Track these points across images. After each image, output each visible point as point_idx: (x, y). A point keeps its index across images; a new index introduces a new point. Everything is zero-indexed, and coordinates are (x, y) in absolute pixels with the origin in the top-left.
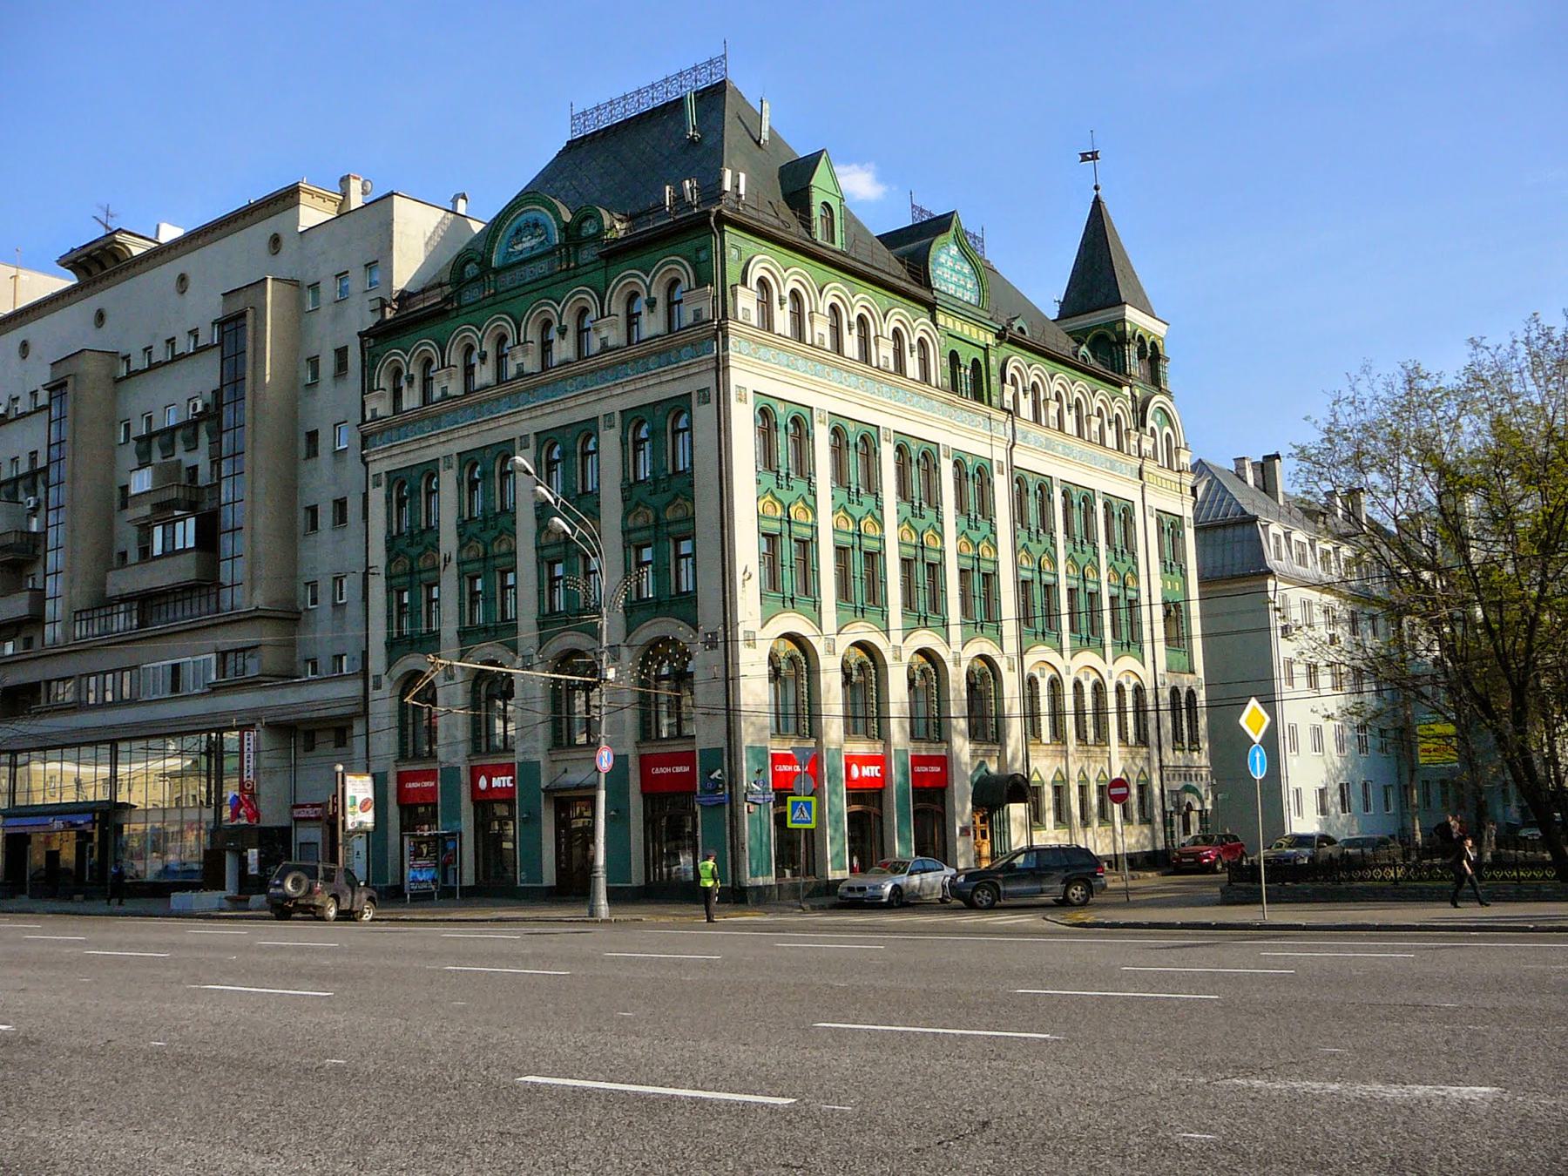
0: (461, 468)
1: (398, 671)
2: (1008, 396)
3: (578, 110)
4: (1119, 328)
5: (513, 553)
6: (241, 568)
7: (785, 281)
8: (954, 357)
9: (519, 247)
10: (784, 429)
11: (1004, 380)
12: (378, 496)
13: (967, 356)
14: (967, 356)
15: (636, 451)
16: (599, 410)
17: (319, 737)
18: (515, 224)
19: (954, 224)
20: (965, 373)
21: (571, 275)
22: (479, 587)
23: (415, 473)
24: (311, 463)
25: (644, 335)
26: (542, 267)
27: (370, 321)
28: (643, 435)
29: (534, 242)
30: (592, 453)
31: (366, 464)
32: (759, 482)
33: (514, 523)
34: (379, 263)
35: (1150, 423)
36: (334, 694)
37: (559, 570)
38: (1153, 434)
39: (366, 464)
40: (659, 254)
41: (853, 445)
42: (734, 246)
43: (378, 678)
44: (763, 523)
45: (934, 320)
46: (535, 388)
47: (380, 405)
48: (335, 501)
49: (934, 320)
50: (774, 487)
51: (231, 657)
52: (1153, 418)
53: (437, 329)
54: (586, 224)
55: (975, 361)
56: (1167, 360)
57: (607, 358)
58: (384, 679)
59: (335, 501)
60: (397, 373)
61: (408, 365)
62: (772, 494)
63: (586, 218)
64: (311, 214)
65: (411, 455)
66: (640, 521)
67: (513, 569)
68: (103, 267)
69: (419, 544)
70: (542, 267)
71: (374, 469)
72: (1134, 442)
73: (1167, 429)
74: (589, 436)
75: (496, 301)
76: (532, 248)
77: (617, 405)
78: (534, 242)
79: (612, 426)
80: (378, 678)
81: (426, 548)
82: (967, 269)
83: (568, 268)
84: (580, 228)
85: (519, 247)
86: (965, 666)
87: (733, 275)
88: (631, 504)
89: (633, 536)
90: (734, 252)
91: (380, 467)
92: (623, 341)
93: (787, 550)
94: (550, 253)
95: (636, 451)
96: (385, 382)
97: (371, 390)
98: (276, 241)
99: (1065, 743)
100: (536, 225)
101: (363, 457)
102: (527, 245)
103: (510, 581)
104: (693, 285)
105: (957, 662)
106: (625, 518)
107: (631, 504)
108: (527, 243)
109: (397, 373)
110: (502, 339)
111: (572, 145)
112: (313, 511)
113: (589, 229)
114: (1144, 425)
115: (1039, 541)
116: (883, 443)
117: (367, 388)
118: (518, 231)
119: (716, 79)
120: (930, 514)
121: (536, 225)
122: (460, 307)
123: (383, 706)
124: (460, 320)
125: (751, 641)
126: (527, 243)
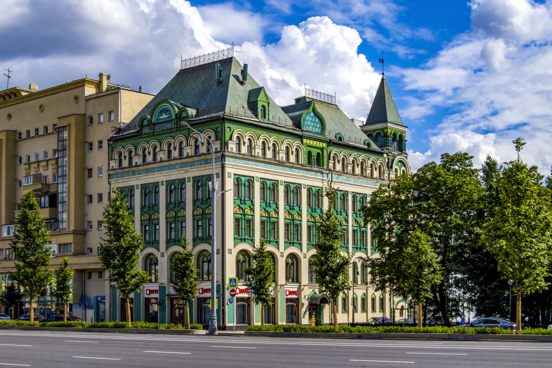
2: (331, 165)
3: (184, 59)
4: (385, 131)
5: (158, 219)
6: (65, 216)
8: (309, 153)
9: (161, 117)
10: (244, 185)
11: (329, 159)
13: (314, 152)
14: (314, 152)
15: (197, 190)
16: (186, 176)
17: (93, 274)
18: (160, 109)
19: (312, 105)
22: (147, 228)
23: (127, 189)
24: (90, 179)
25: (200, 152)
26: (169, 125)
27: (112, 134)
28: (200, 184)
29: (167, 116)
31: (110, 184)
32: (234, 202)
35: (395, 166)
37: (173, 225)
38: (396, 170)
39: (110, 184)
40: (205, 128)
41: (270, 188)
44: (235, 215)
45: (302, 142)
47: (114, 164)
48: (98, 194)
49: (302, 142)
50: (239, 204)
53: (134, 141)
55: (318, 154)
56: (406, 141)
57: (188, 160)
59: (98, 194)
60: (120, 154)
61: (124, 152)
62: (239, 206)
63: (183, 111)
64: (90, 90)
65: (125, 183)
66: (198, 213)
67: (158, 224)
68: (10, 98)
69: (206, 203)
70: (169, 125)
71: (227, 170)
72: (386, 175)
73: (403, 168)
75: (153, 135)
76: (166, 118)
77: (139, 182)
78: (167, 116)
82: (317, 120)
83: (177, 127)
84: (181, 114)
85: (161, 117)
86: (308, 257)
87: (227, 138)
88: (195, 207)
92: (193, 154)
93: (243, 224)
94: (171, 121)
95: (197, 190)
96: (117, 157)
97: (112, 159)
98: (76, 98)
102: (164, 117)
103: (157, 227)
105: (305, 257)
106: (193, 212)
107: (195, 207)
108: (164, 116)
109: (120, 154)
110: (155, 148)
112: (91, 197)
113: (184, 115)
114: (391, 167)
115: (341, 215)
116: (280, 186)
117: (110, 158)
120: (297, 209)
122: (142, 134)
124: (142, 140)
126: (164, 116)
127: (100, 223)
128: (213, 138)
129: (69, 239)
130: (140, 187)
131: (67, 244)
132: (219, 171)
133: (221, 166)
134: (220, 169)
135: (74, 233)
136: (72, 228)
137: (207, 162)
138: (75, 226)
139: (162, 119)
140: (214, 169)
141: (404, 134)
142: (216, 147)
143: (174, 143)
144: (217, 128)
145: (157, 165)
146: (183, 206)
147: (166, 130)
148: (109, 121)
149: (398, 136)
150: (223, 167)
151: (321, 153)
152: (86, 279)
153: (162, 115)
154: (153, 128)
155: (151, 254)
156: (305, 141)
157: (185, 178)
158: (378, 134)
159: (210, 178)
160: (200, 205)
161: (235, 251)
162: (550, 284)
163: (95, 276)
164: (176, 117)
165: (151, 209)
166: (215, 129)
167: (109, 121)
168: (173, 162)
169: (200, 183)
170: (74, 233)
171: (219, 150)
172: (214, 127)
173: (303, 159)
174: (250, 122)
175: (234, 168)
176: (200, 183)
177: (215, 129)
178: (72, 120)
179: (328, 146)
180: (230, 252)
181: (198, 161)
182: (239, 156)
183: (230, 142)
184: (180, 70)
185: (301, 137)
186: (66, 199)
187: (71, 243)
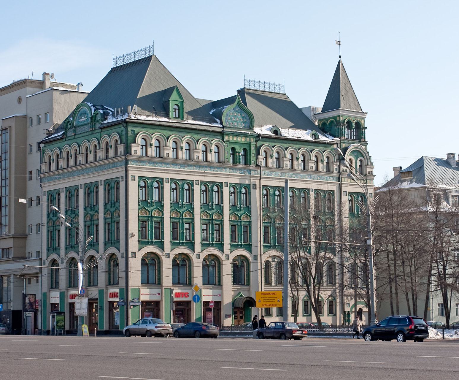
0: (66, 192)
1: (50, 259)
3: (115, 57)
4: (338, 119)
8: (233, 149)
9: (81, 120)
12: (45, 199)
24: (31, 181)
31: (42, 187)
33: (119, 206)
34: (49, 113)
36: (33, 265)
39: (42, 187)
43: (45, 261)
46: (83, 170)
49: (223, 139)
51: (5, 250)
58: (46, 261)
65: (54, 186)
69: (114, 207)
71: (131, 173)
77: (103, 178)
80: (45, 261)
81: (76, 216)
83: (92, 131)
85: (81, 120)
91: (45, 189)
99: (335, 315)
101: (41, 186)
102: (83, 120)
107: (106, 210)
111: (114, 70)
118: (81, 114)
121: (85, 113)
123: (46, 268)
124: (66, 142)
125: (134, 255)
126: (83, 119)
127: (39, 226)
128: (119, 142)
129: (9, 243)
130: (64, 189)
131: (8, 248)
133: (124, 169)
134: (124, 172)
135: (14, 237)
136: (12, 232)
137: (114, 165)
138: (15, 230)
140: (119, 173)
141: (363, 122)
144: (122, 131)
145: (79, 169)
146: (97, 210)
148: (45, 123)
149: (354, 124)
151: (248, 149)
152: (27, 285)
154: (75, 131)
155: (113, 254)
156: (226, 138)
158: (332, 122)
160: (109, 208)
161: (140, 255)
162: (283, 287)
163: (34, 280)
164: (92, 121)
165: (113, 205)
166: (120, 132)
167: (45, 123)
168: (80, 167)
169: (112, 186)
170: (14, 237)
172: (119, 130)
173: (226, 155)
174: (158, 123)
175: (136, 171)
176: (112, 186)
177: (120, 132)
178: (12, 124)
179: (256, 141)
180: (134, 255)
181: (107, 164)
182: (145, 159)
183: (133, 145)
184: (112, 69)
185: (222, 134)
186: (7, 203)
187: (12, 248)
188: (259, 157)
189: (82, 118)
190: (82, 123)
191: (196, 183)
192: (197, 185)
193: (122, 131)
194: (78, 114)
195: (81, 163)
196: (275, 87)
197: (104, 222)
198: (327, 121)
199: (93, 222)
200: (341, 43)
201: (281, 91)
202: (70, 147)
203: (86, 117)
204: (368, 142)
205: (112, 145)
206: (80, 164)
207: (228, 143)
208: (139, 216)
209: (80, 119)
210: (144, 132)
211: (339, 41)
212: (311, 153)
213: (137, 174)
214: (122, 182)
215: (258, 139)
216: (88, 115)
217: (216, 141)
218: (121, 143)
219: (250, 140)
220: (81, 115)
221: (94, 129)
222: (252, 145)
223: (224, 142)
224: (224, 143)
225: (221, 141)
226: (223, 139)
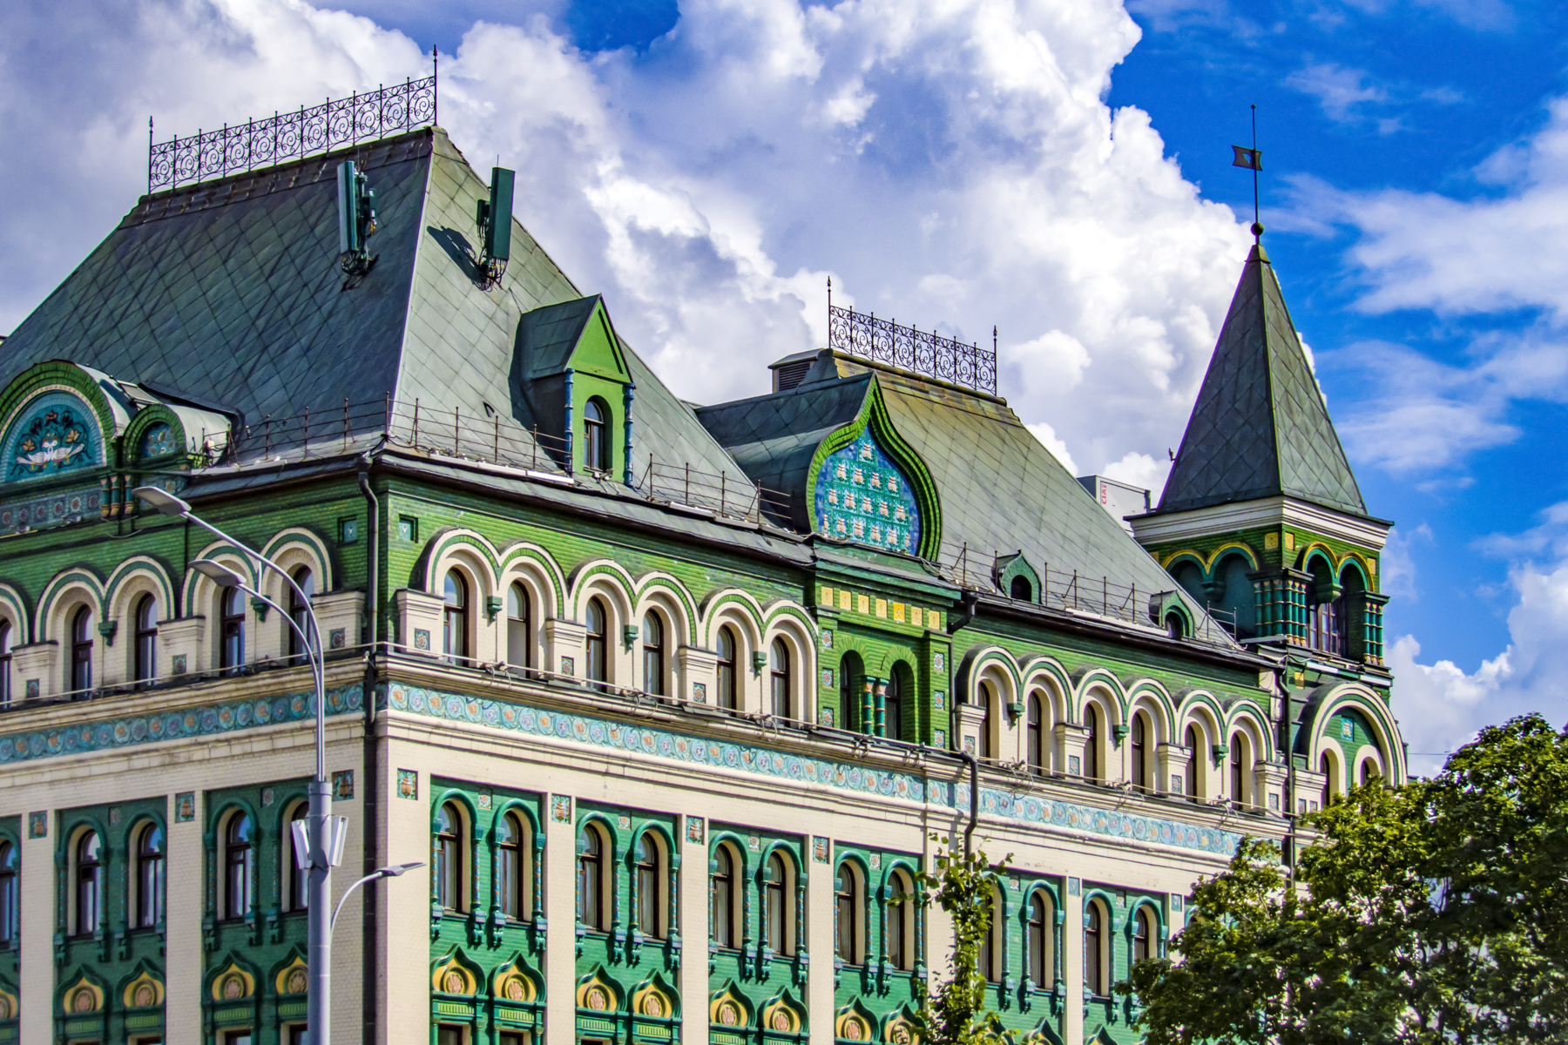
3: (163, 136)
4: (1270, 543)
7: (498, 570)
8: (851, 662)
9: (36, 459)
10: (486, 840)
11: (961, 697)
13: (879, 659)
14: (879, 659)
15: (231, 864)
16: (168, 784)
18: (30, 415)
19: (869, 399)
20: (876, 697)
21: (131, 520)
29: (64, 453)
30: (157, 857)
33: (17, 968)
35: (1321, 742)
40: (276, 519)
42: (403, 518)
44: (440, 1006)
49: (809, 602)
52: (1332, 731)
54: (157, 436)
55: (900, 668)
56: (1381, 601)
57: (182, 698)
69: (279, 940)
70: (76, 503)
71: (397, 755)
72: (1273, 788)
73: (1367, 751)
74: (150, 827)
76: (61, 464)
79: (189, 817)
82: (894, 482)
83: (121, 515)
84: (143, 441)
85: (36, 459)
87: (398, 576)
88: (218, 959)
89: (221, 1016)
90: (405, 528)
95: (231, 864)
100: (68, 423)
104: (330, 588)
108: (52, 453)
111: (155, 211)
113: (161, 447)
114: (1302, 747)
115: (1024, 1007)
116: (687, 846)
118: (36, 428)
119: (419, 123)
121: (68, 423)
126: (52, 453)
128: (319, 578)
132: (354, 758)
133: (360, 731)
139: (40, 469)
140: (326, 749)
141: (1370, 564)
142: (336, 624)
143: (106, 603)
144: (341, 522)
147: (58, 529)
149: (1336, 576)
150: (373, 740)
151: (913, 662)
153: (38, 448)
156: (825, 596)
157: (162, 800)
159: (299, 796)
164: (119, 460)
166: (331, 527)
168: (99, 710)
171: (350, 641)
173: (817, 696)
175: (432, 744)
176: (250, 825)
181: (233, 704)
182: (462, 678)
183: (412, 597)
184: (144, 201)
185: (805, 577)
188: (964, 709)
189: (42, 450)
190: (42, 477)
191: (691, 829)
192: (694, 840)
193: (341, 522)
194: (13, 425)
195: (44, 693)
196: (960, 358)
197: (204, 1024)
198: (1206, 556)
199: (116, 1024)
200: (1262, 161)
201: (984, 384)
202: (104, 582)
203: (76, 443)
204: (1391, 673)
205: (115, 624)
206: (180, 680)
207: (833, 625)
208: (433, 997)
209: (33, 452)
210: (460, 532)
211: (1253, 153)
212: (1177, 707)
213: (431, 761)
214: (186, 826)
215: (957, 617)
216: (85, 429)
217: (782, 604)
218: (339, 586)
219: (925, 620)
220: (34, 431)
221: (129, 508)
222: (933, 646)
223: (815, 617)
224: (816, 627)
225: (803, 610)
226: (809, 602)
